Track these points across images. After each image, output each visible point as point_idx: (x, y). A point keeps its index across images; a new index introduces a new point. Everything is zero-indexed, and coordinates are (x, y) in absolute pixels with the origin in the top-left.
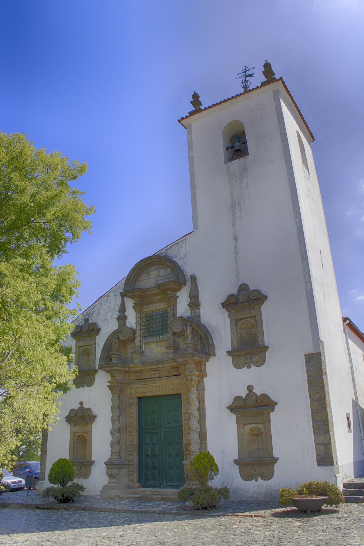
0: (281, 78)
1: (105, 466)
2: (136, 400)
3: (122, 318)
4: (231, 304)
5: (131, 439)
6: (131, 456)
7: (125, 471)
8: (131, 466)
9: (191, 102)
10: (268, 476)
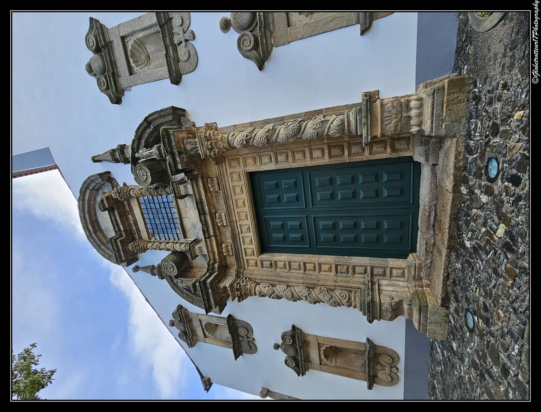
2: (265, 256)
5: (325, 267)
6: (357, 269)
7: (384, 282)
8: (376, 271)
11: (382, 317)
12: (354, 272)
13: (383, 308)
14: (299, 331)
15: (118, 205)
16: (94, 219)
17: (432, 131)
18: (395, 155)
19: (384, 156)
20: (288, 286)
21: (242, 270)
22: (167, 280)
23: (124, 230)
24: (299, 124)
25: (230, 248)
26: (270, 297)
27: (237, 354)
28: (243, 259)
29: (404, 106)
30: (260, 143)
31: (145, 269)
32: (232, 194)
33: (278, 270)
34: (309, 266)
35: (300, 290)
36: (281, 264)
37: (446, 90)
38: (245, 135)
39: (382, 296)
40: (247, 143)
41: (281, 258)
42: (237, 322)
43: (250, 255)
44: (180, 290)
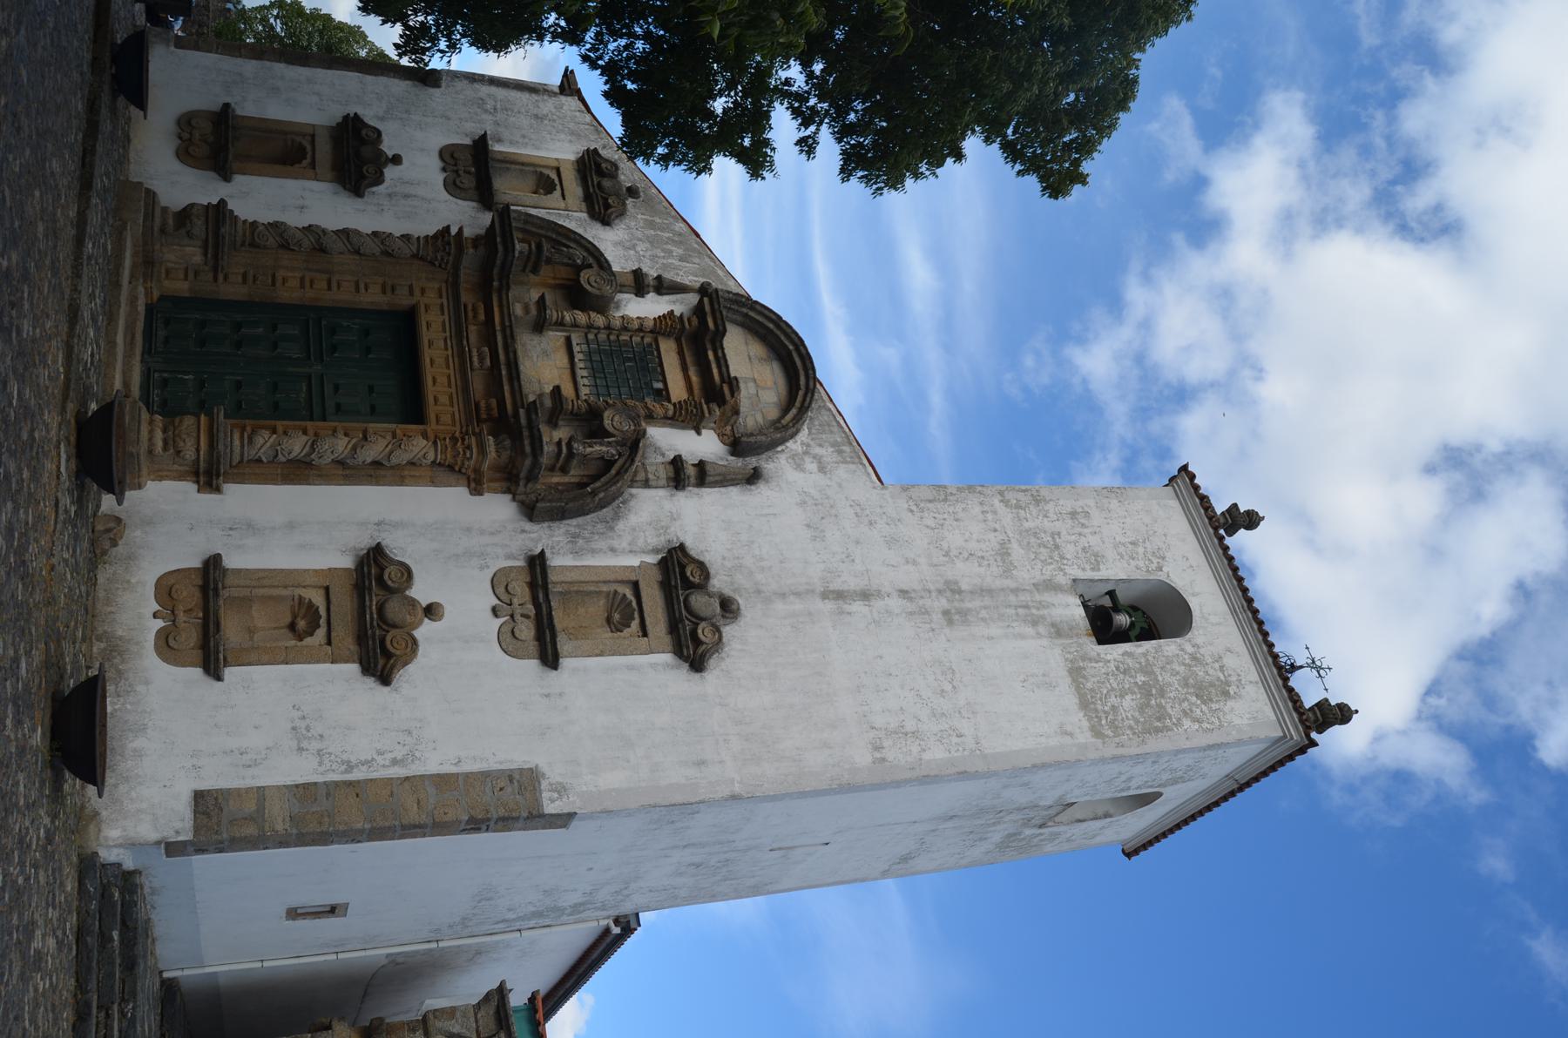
0: (1313, 744)
2: (405, 301)
3: (639, 284)
4: (679, 570)
5: (294, 283)
6: (240, 279)
7: (198, 259)
8: (211, 276)
9: (1235, 506)
10: (167, 646)
22: (123, 160)
25: (470, 314)
27: (481, 144)
41: (373, 297)
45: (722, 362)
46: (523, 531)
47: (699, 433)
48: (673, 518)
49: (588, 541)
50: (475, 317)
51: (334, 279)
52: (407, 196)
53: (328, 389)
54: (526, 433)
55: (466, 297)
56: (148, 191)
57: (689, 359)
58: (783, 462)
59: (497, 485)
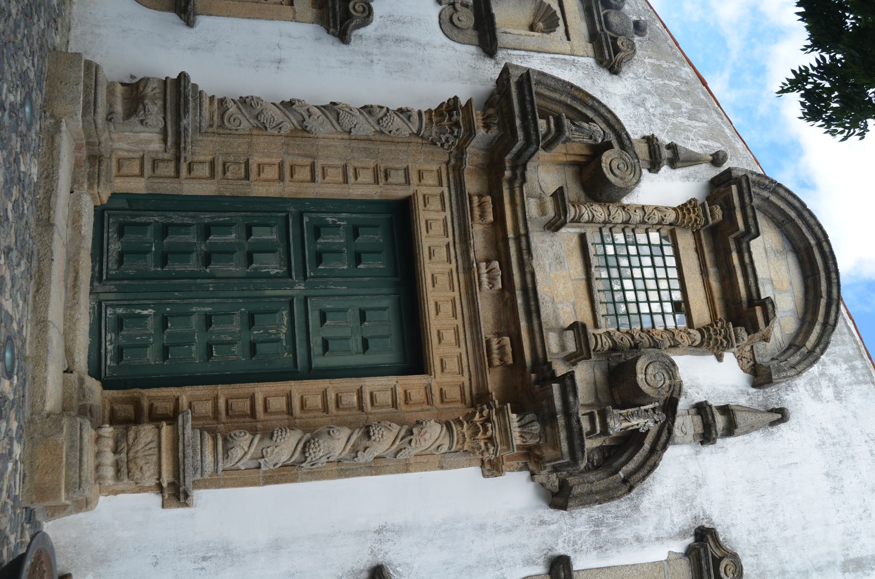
1: (174, 76)
2: (401, 193)
5: (271, 173)
6: (206, 171)
7: (156, 146)
8: (170, 170)
11: (162, 85)
12: (212, 164)
13: (160, 103)
14: (332, 30)
15: (739, 313)
16: (810, 281)
17: (81, 425)
18: (136, 392)
19: (154, 392)
20: (350, 132)
21: (453, 162)
23: (731, 252)
24: (306, 458)
25: (477, 212)
26: (388, 110)
28: (449, 187)
29: (124, 470)
30: (385, 427)
31: (693, 160)
32: (461, 330)
33: (372, 164)
34: (305, 174)
35: (321, 127)
36: (366, 176)
37: (63, 486)
38: (413, 444)
39: (161, 125)
40: (411, 429)
41: (364, 189)
42: (475, 40)
43: (433, 196)
44: (600, 115)
45: (749, 269)
46: (543, 523)
47: (720, 358)
48: (699, 484)
49: (613, 529)
50: (482, 216)
51: (319, 164)
52: (399, 40)
53: (314, 317)
54: (561, 421)
55: (472, 185)
56: (89, 64)
57: (708, 257)
58: (802, 389)
59: (514, 463)
